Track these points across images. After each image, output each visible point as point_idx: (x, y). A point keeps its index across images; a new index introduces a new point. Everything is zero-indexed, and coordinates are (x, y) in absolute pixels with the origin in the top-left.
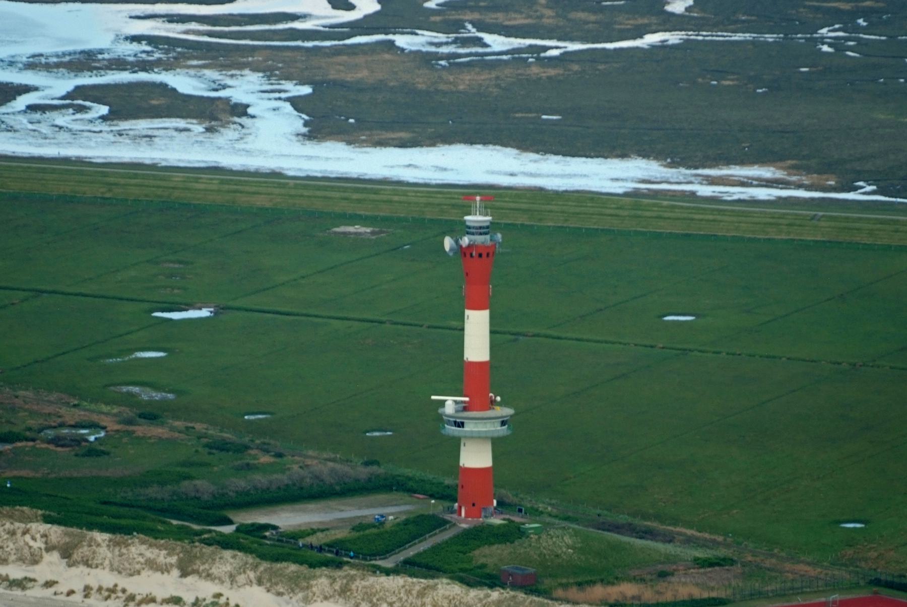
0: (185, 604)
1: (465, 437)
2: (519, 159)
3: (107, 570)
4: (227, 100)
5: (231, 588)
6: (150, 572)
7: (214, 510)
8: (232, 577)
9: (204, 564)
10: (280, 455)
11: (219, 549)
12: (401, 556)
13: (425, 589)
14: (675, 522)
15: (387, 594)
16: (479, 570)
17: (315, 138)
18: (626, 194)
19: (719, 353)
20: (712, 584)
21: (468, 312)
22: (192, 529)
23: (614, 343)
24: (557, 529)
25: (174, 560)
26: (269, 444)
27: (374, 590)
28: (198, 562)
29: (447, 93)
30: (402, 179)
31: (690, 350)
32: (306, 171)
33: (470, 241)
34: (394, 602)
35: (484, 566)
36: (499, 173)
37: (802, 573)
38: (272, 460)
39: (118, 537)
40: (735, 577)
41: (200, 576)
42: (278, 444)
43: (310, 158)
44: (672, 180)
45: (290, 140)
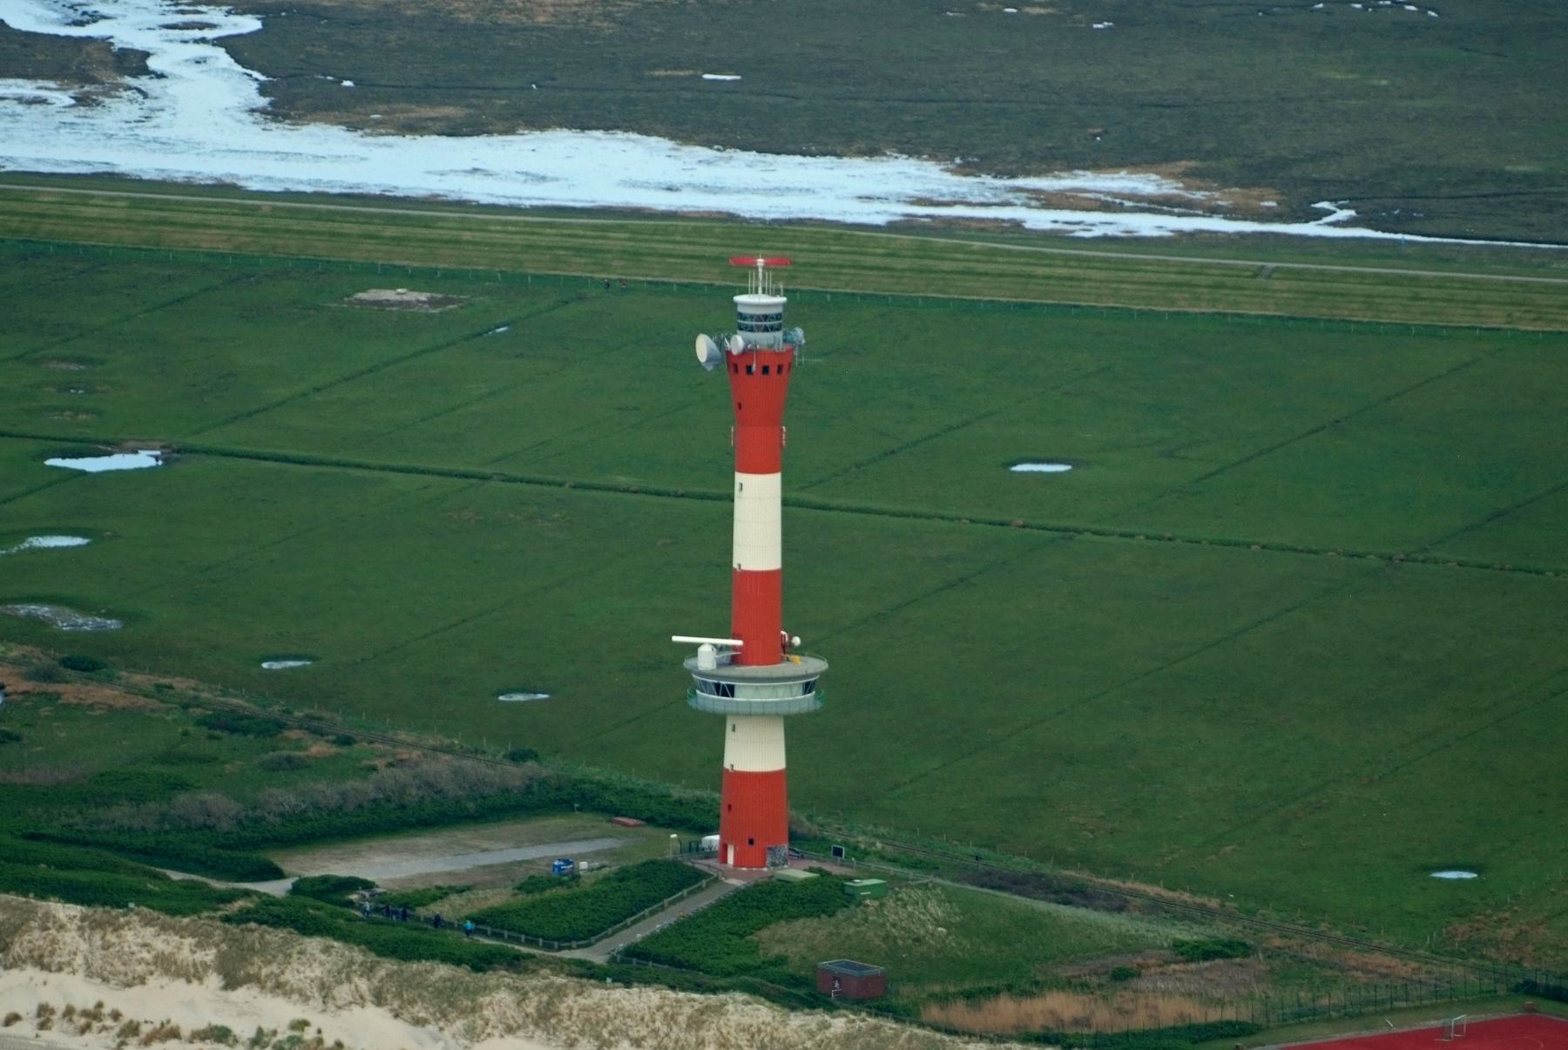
0: (236, 1041)
1: (738, 714)
2: (676, 157)
3: (81, 975)
4: (105, 43)
5: (324, 1011)
6: (165, 980)
7: (245, 850)
8: (325, 990)
9: (269, 963)
10: (347, 741)
11: (296, 936)
12: (621, 941)
13: (702, 1012)
14: (1122, 870)
15: (629, 1021)
16: (772, 969)
17: (286, 117)
18: (892, 227)
19: (1132, 536)
20: (1218, 993)
21: (740, 477)
22: (213, 890)
23: (929, 517)
24: (912, 887)
25: (209, 955)
26: (320, 719)
27: (603, 1016)
28: (256, 960)
29: (516, 30)
30: (466, 197)
31: (1076, 531)
32: (280, 181)
33: (747, 342)
34: (644, 1038)
35: (781, 960)
36: (645, 185)
37: (1383, 971)
38: (334, 749)
39: (99, 912)
40: (1259, 980)
41: (263, 988)
42: (339, 718)
43: (284, 156)
44: (971, 199)
45: (240, 121)
